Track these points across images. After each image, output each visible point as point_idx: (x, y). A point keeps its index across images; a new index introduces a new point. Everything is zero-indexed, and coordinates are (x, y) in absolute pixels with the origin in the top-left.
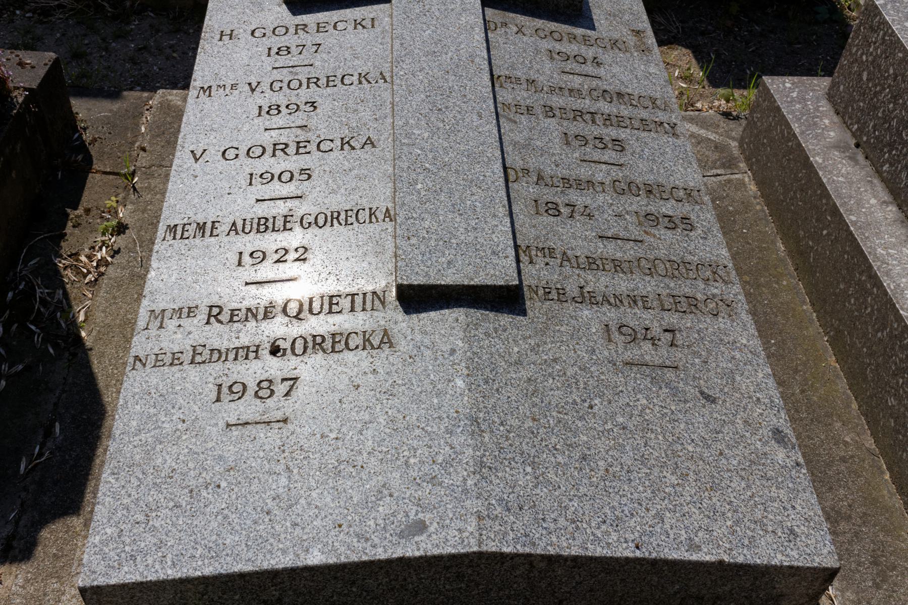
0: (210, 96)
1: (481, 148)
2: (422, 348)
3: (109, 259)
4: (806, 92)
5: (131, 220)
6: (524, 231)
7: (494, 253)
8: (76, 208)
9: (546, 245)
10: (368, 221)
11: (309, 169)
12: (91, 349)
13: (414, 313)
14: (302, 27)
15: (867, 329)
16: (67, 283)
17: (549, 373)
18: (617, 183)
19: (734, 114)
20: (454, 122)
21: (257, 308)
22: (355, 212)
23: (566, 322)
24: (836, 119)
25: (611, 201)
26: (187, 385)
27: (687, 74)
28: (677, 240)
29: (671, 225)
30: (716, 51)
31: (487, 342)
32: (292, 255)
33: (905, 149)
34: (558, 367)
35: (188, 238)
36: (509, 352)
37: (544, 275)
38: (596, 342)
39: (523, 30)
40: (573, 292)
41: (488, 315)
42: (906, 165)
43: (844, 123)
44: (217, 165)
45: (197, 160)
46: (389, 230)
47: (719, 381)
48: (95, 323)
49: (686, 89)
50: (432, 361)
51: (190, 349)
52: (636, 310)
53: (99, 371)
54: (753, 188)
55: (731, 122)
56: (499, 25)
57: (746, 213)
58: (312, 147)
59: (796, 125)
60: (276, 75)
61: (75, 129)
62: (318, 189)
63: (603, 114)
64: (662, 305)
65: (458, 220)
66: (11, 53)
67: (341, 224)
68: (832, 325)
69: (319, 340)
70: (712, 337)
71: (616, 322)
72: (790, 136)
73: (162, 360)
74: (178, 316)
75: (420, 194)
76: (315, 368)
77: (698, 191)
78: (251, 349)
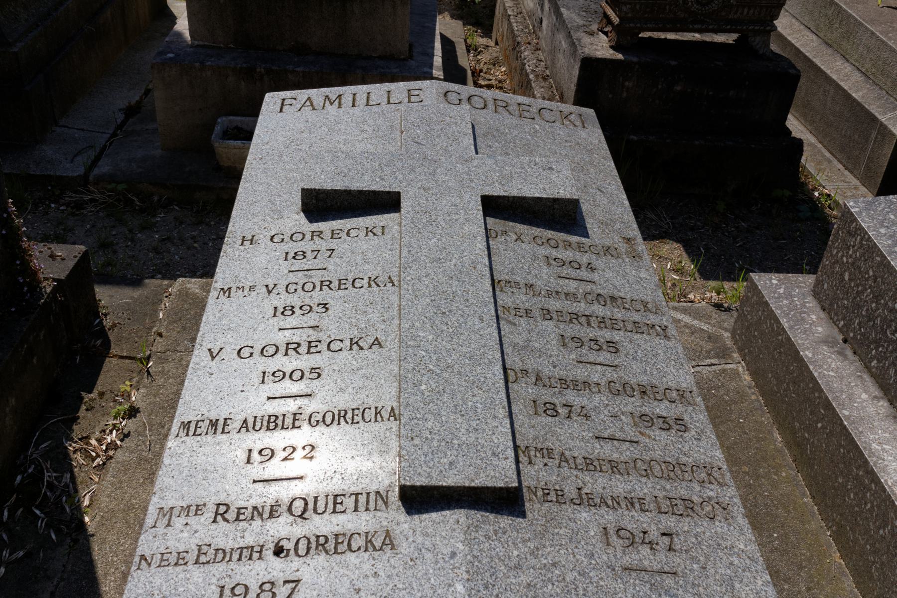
0: (229, 297)
1: (482, 350)
2: (423, 550)
3: (118, 442)
4: (792, 289)
5: (143, 403)
6: (523, 432)
7: (494, 454)
8: (90, 392)
9: (544, 446)
10: (373, 420)
11: (319, 368)
12: (93, 535)
13: (416, 514)
14: (318, 233)
15: (869, 525)
16: (76, 467)
17: (549, 578)
18: (612, 384)
19: (726, 305)
20: (457, 325)
21: (263, 507)
22: (361, 411)
23: (565, 525)
24: (822, 315)
25: (606, 402)
26: (190, 586)
27: (679, 266)
28: (672, 441)
29: (666, 426)
30: (705, 245)
31: (487, 545)
32: (300, 453)
33: (891, 347)
34: (557, 572)
35: (200, 435)
36: (509, 556)
37: (543, 476)
38: (594, 545)
39: (521, 237)
40: (571, 493)
41: (488, 516)
42: (893, 363)
43: (831, 319)
44: (232, 363)
45: (213, 358)
46: (394, 430)
47: (718, 588)
48: (99, 508)
49: (678, 281)
50: (432, 565)
51: (196, 548)
52: (634, 513)
53: (99, 559)
54: (747, 377)
55: (723, 313)
56: (500, 233)
57: (742, 402)
58: (323, 347)
59: (785, 320)
60: (292, 278)
61: (96, 315)
62: (327, 387)
63: (597, 317)
64: (659, 508)
65: (460, 420)
66: (44, 246)
67: (347, 423)
68: (834, 520)
69: (322, 540)
70: (710, 542)
71: (614, 524)
72: (780, 331)
73: (167, 560)
74: (186, 514)
75: (424, 394)
76: (318, 570)
77: (691, 392)
78: (255, 549)
